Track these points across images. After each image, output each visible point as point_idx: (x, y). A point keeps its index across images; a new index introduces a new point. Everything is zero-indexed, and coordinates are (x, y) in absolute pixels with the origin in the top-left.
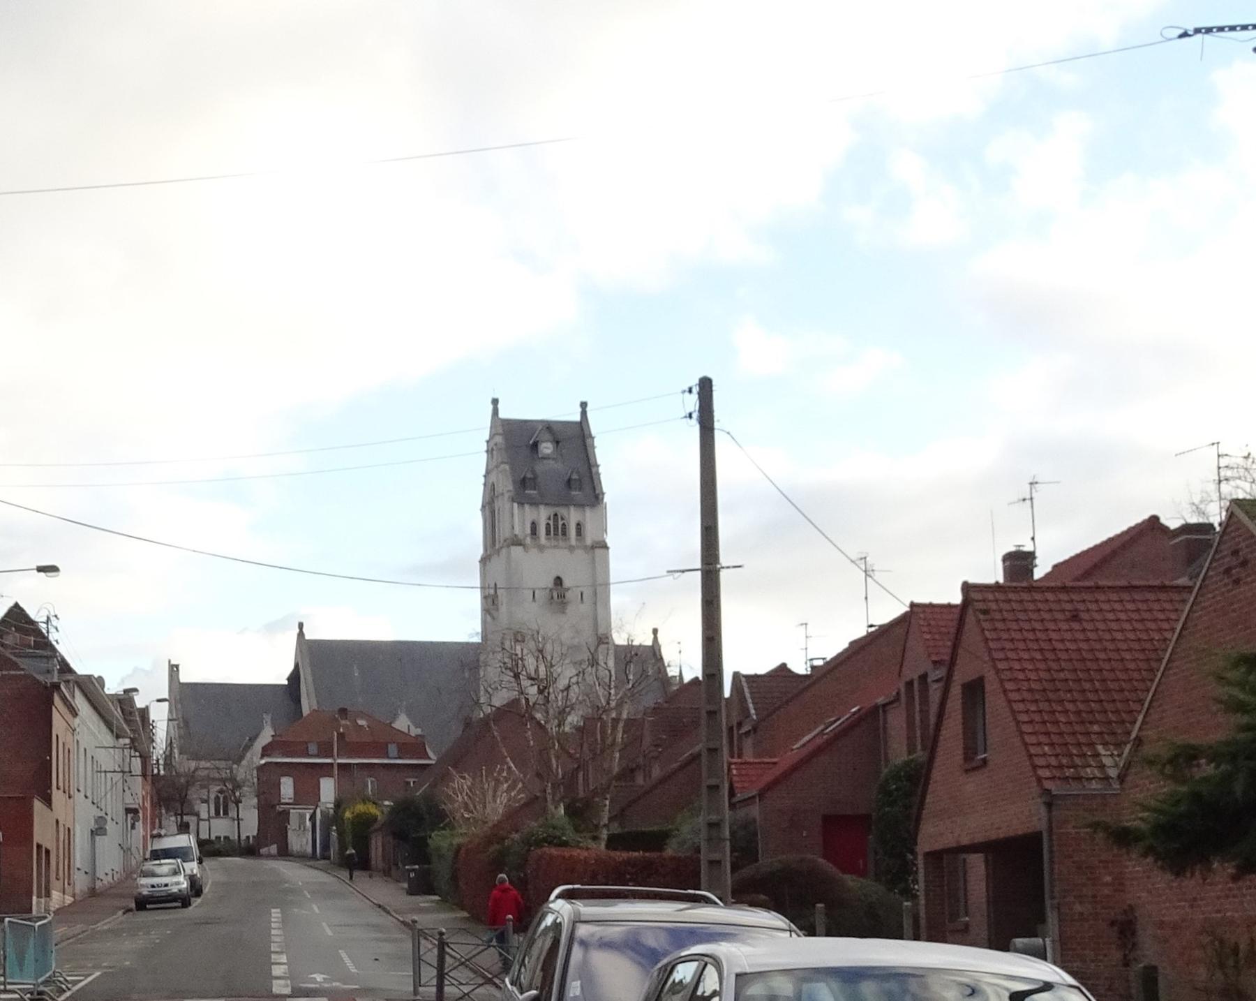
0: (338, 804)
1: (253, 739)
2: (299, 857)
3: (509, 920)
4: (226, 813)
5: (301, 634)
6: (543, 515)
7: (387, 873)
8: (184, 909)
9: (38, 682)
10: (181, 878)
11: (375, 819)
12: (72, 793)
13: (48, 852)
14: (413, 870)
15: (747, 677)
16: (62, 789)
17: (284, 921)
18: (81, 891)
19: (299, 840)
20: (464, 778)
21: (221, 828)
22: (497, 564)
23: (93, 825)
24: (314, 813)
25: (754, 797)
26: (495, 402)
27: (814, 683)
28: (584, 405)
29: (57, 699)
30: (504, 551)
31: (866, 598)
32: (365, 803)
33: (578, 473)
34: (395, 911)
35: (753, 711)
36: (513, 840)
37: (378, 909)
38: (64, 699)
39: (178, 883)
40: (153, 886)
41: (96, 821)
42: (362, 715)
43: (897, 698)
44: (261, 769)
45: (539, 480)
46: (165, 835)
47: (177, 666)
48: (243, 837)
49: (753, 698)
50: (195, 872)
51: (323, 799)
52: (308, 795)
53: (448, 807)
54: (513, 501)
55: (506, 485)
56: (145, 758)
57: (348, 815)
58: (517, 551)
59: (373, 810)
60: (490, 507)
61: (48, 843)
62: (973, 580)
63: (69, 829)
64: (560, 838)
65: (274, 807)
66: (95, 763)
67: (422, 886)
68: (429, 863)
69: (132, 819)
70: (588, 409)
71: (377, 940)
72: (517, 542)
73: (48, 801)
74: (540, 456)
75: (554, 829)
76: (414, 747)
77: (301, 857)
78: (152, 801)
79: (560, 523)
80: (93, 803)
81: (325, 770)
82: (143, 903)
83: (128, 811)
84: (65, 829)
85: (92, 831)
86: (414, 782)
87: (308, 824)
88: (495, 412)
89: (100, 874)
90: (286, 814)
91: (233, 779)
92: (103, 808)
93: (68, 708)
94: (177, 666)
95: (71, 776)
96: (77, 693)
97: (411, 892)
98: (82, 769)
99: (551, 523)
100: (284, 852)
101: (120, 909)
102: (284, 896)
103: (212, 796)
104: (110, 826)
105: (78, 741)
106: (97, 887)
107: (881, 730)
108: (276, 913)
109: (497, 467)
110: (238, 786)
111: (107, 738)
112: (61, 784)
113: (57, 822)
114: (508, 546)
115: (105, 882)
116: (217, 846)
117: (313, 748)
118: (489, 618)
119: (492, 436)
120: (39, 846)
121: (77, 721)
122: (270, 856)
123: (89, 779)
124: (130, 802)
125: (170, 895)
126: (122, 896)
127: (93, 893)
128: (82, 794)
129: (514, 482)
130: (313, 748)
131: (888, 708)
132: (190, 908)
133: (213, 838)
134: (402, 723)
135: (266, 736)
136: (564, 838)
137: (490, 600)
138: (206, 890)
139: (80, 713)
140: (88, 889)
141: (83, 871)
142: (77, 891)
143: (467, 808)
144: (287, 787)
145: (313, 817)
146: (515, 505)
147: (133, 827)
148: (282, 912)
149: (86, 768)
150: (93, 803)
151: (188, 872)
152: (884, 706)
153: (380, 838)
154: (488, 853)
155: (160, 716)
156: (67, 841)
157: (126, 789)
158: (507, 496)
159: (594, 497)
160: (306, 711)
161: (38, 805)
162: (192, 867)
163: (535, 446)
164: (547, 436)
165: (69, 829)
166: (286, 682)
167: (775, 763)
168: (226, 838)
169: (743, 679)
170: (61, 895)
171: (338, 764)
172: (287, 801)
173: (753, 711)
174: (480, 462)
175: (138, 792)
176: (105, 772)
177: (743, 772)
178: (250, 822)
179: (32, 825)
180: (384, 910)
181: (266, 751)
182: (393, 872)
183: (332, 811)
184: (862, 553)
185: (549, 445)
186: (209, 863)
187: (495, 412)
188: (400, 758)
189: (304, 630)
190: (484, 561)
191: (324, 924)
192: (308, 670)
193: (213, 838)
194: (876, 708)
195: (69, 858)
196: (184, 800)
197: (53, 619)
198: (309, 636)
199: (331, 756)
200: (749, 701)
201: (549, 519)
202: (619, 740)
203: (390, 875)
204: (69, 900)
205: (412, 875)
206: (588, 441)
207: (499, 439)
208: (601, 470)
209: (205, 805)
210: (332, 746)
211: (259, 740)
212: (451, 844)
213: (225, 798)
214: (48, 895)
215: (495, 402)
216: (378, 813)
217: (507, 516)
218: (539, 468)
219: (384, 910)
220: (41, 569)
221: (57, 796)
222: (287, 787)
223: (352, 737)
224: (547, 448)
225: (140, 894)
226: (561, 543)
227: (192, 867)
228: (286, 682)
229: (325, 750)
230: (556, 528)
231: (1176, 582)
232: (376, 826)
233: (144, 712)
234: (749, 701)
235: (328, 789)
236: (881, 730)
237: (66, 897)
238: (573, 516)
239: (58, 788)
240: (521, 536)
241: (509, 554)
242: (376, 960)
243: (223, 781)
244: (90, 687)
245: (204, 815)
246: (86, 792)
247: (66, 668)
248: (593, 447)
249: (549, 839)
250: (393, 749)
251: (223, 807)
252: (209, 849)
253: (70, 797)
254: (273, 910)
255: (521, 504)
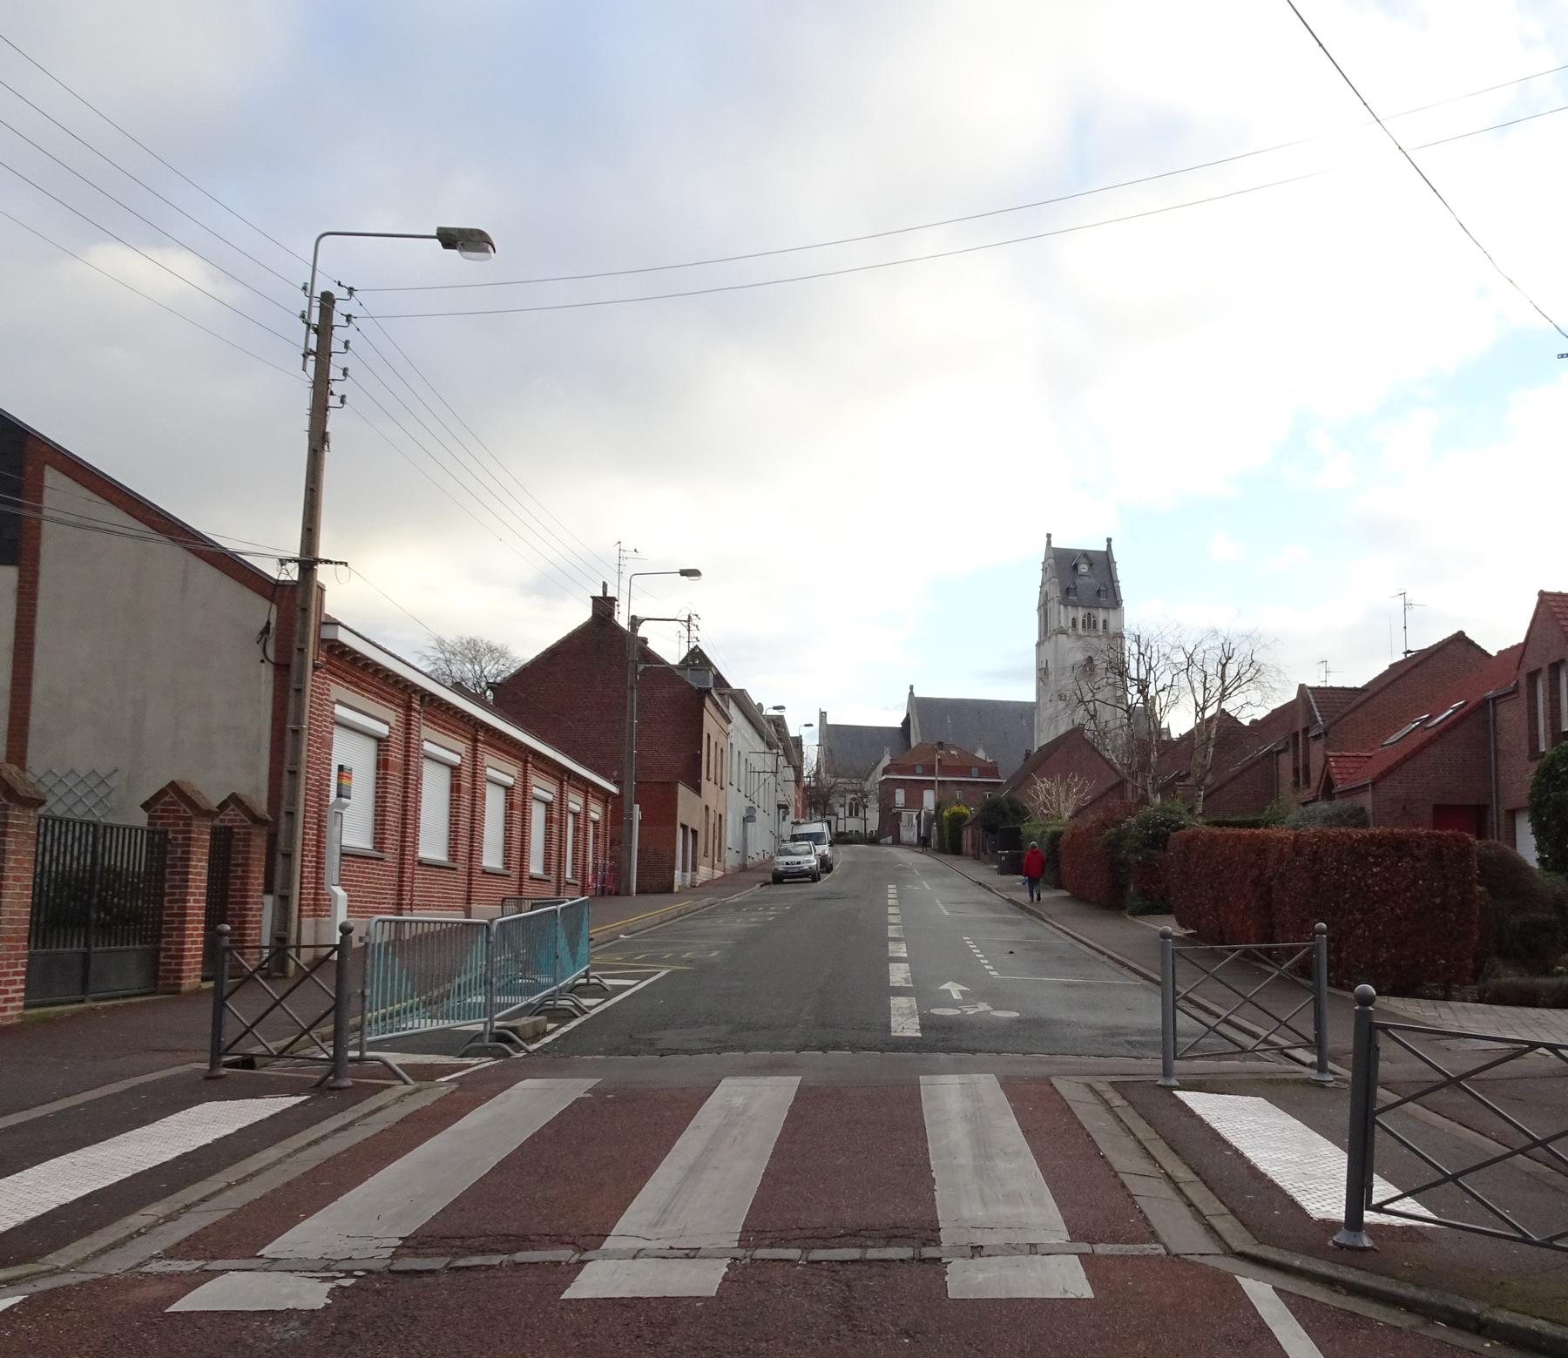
0: (938, 807)
1: (878, 763)
2: (908, 845)
3: (1321, 932)
4: (857, 814)
5: (911, 693)
6: (1080, 614)
7: (976, 857)
8: (815, 884)
9: (692, 687)
10: (812, 857)
11: (966, 817)
12: (724, 785)
13: (694, 832)
14: (1003, 855)
15: (1311, 688)
16: (713, 780)
17: (899, 898)
18: (732, 866)
19: (909, 833)
20: (1043, 782)
21: (853, 825)
22: (1049, 646)
23: (744, 814)
24: (920, 813)
25: (1367, 785)
26: (1049, 536)
27: (1373, 696)
28: (1109, 540)
29: (708, 702)
30: (1053, 638)
31: (1405, 628)
32: (959, 806)
33: (1105, 585)
34: (997, 889)
35: (1319, 718)
36: (1129, 823)
37: (980, 887)
38: (716, 704)
39: (809, 861)
40: (787, 864)
41: (747, 811)
42: (955, 748)
43: (1516, 690)
44: (881, 783)
45: (1078, 590)
46: (803, 823)
47: (825, 713)
48: (868, 831)
49: (1318, 707)
50: (826, 853)
51: (925, 805)
52: (914, 801)
53: (1029, 805)
54: (1060, 604)
55: (1055, 593)
56: (798, 770)
57: (946, 813)
58: (1062, 638)
59: (965, 811)
60: (1044, 608)
61: (695, 822)
62: (1548, 589)
63: (720, 816)
64: (1177, 822)
65: (890, 809)
66: (749, 764)
67: (1010, 868)
68: (1021, 849)
69: (784, 812)
70: (1112, 543)
71: (994, 921)
72: (1062, 632)
73: (697, 789)
74: (1079, 573)
75: (1170, 813)
76: (991, 770)
77: (910, 845)
78: (803, 803)
79: (1092, 620)
80: (746, 796)
81: (929, 785)
82: (779, 878)
83: (780, 807)
84: (715, 814)
85: (744, 819)
86: (990, 795)
87: (915, 821)
88: (1049, 543)
89: (751, 853)
90: (899, 814)
91: (861, 791)
92: (756, 801)
93: (721, 713)
94: (825, 713)
95: (724, 771)
96: (732, 705)
97: (1002, 872)
98: (735, 767)
99: (1086, 620)
100: (897, 842)
101: (758, 882)
102: (898, 874)
103: (848, 801)
104: (759, 814)
105: (731, 744)
106: (748, 863)
107: (1491, 723)
108: (892, 889)
109: (1050, 580)
110: (866, 796)
111: (760, 746)
112: (712, 776)
113: (707, 808)
114: (1056, 634)
115: (756, 859)
116: (850, 837)
117: (919, 770)
118: (1041, 684)
119: (1046, 560)
120: (684, 827)
121: (731, 726)
122: (887, 844)
123: (742, 777)
124: (782, 799)
125: (802, 871)
126: (764, 871)
127: (743, 868)
128: (735, 787)
129: (1061, 590)
130: (919, 770)
131: (1498, 702)
132: (819, 883)
133: (847, 831)
134: (981, 754)
135: (886, 761)
136: (1182, 823)
137: (1043, 671)
138: (836, 867)
139: (733, 721)
140: (739, 865)
141: (734, 850)
142: (728, 867)
143: (1046, 807)
144: (900, 797)
145: (918, 817)
146: (1062, 606)
147: (784, 819)
148: (897, 889)
149: (739, 768)
150: (746, 796)
151: (819, 852)
152: (1494, 699)
153: (970, 831)
154: (1104, 836)
155: (811, 752)
156: (717, 826)
157: (779, 790)
158: (1056, 599)
159: (1115, 603)
160: (914, 744)
161: (683, 791)
162: (824, 849)
163: (1076, 567)
164: (1084, 560)
165: (720, 816)
166: (901, 726)
167: (1370, 757)
168: (857, 831)
169: (1309, 691)
170: (711, 869)
171: (939, 781)
172: (900, 806)
173: (1319, 718)
174: (1037, 576)
175: (790, 794)
176: (759, 772)
177: (1341, 765)
178: (873, 819)
179: (676, 806)
180: (985, 886)
181: (886, 771)
182: (982, 855)
183: (933, 812)
184: (1400, 589)
185: (1085, 566)
186: (841, 849)
187: (1049, 543)
188: (979, 778)
189: (914, 690)
190: (1039, 645)
191: (938, 902)
192: (916, 718)
193: (847, 831)
194: (1486, 701)
195: (720, 839)
196: (826, 804)
197: (693, 617)
198: (917, 694)
199: (933, 775)
200: (1316, 709)
201: (1085, 616)
202: (1213, 736)
203: (978, 859)
204: (718, 874)
205: (1003, 858)
206: (1112, 565)
207: (1051, 561)
208: (1120, 584)
209: (842, 809)
210: (934, 766)
211: (880, 764)
212: (1044, 832)
213: (856, 804)
214: (695, 869)
215: (1049, 536)
216: (969, 813)
217: (1056, 614)
218: (1078, 581)
219: (985, 886)
220: (684, 573)
221: (706, 786)
222: (900, 797)
223: (946, 763)
224: (1084, 568)
225: (776, 870)
226: (1093, 634)
227: (824, 849)
228: (901, 726)
229: (929, 770)
230: (1089, 625)
231: (929, 861)
232: (966, 822)
233: (798, 741)
234: (1316, 709)
235: (929, 799)
236: (1491, 723)
237: (716, 871)
238: (1101, 615)
239: (708, 779)
240: (1065, 628)
241: (1057, 638)
242: (1011, 953)
243: (855, 792)
244: (740, 699)
245: (841, 815)
246: (739, 785)
247: (720, 681)
248: (1115, 569)
249: (1167, 823)
250: (975, 771)
251: (854, 810)
252: (840, 839)
253: (722, 789)
254: (889, 886)
255: (1065, 606)
